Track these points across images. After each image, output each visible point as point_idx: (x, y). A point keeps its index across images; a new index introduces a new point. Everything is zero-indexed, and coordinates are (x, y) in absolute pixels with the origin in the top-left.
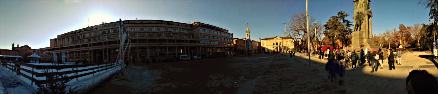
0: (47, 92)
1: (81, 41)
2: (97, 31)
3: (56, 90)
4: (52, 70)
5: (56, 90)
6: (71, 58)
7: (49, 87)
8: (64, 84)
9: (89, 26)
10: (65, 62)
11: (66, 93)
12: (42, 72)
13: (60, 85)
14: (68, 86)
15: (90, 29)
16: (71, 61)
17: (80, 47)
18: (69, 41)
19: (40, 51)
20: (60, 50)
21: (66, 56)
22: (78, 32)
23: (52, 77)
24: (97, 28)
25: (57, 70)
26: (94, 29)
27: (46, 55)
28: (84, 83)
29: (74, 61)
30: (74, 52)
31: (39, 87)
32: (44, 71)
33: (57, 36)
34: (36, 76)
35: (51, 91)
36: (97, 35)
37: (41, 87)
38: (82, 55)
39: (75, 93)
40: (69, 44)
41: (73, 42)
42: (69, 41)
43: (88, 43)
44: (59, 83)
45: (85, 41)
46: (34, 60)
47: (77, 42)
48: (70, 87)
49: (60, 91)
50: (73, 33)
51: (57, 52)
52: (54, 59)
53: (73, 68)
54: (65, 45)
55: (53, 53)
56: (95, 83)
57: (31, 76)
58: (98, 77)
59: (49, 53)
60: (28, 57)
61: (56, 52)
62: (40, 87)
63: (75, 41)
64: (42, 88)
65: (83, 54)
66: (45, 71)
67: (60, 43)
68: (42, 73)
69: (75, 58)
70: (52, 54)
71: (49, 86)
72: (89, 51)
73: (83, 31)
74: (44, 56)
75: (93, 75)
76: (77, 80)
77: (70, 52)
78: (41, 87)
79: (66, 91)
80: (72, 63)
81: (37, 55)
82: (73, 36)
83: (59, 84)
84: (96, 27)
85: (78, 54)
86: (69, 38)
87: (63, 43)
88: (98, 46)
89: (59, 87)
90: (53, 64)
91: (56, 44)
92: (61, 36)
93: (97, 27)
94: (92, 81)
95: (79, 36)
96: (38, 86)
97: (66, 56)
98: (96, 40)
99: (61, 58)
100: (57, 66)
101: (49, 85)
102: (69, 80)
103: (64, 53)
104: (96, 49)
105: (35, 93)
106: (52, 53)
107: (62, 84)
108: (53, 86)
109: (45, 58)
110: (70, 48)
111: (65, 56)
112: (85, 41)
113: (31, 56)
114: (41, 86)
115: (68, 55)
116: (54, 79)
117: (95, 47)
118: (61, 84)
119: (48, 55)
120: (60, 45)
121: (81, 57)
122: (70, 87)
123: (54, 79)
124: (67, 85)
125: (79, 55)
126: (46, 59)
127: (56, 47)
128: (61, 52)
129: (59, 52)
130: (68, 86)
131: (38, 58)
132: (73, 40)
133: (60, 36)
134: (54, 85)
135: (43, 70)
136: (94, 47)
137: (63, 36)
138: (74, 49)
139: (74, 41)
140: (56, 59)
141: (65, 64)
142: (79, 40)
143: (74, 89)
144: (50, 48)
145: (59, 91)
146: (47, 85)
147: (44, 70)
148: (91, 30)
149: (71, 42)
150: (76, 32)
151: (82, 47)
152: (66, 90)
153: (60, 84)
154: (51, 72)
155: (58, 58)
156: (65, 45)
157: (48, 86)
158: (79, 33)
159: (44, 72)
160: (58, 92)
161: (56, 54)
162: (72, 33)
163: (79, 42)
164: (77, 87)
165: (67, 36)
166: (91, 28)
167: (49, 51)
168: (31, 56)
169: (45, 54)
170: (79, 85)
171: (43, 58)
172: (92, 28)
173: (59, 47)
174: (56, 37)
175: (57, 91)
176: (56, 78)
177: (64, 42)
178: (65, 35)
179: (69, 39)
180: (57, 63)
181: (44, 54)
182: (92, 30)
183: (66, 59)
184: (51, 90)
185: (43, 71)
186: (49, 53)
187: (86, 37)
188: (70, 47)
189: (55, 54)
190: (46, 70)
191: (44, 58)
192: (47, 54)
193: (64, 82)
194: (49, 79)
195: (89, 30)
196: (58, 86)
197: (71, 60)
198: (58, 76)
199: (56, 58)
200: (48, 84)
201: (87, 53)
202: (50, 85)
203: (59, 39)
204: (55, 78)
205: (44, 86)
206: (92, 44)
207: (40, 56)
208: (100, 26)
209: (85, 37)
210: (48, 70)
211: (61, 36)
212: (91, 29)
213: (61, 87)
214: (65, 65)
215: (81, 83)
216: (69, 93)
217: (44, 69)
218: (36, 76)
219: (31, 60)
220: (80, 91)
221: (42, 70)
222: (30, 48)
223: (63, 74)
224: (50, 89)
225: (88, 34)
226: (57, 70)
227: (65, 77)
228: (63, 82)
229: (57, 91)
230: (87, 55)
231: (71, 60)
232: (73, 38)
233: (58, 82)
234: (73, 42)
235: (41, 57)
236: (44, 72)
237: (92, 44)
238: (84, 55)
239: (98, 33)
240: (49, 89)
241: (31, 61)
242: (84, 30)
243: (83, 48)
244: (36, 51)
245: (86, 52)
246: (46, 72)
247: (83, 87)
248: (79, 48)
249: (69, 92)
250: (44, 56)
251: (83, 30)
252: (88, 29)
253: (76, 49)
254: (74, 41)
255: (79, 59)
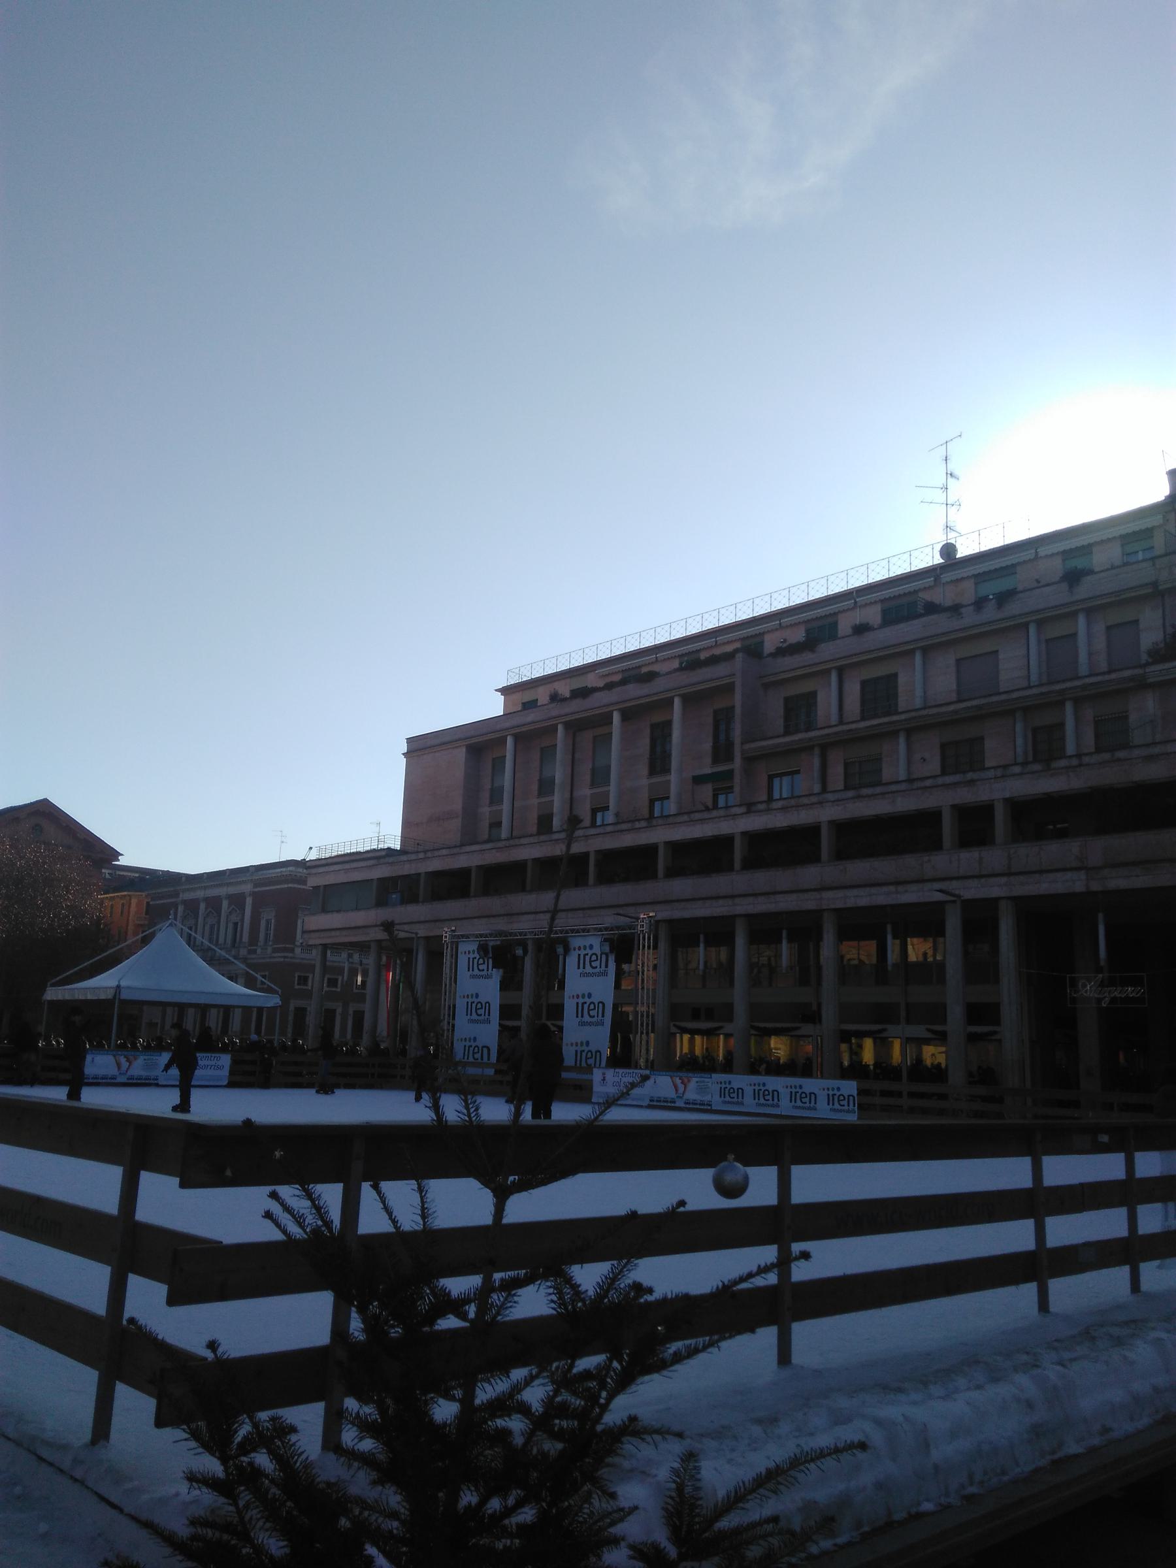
0: (344, 1522)
1: (837, 773)
2: (1090, 612)
3: (469, 1498)
4: (416, 1198)
5: (469, 1498)
6: (696, 1014)
7: (368, 1445)
8: (594, 1406)
9: (962, 552)
10: (606, 1081)
11: (615, 1541)
12: (268, 1215)
13: (541, 1423)
14: (663, 1432)
15: (968, 592)
16: (691, 1065)
17: (815, 858)
18: (659, 763)
19: (260, 901)
20: (546, 899)
21: (617, 985)
22: (798, 635)
23: (423, 1306)
24: (1079, 563)
25: (502, 1195)
26: (1039, 584)
27: (339, 959)
28: (892, 1411)
29: (728, 1066)
30: (730, 920)
31: (208, 1448)
32: (301, 1205)
33: (506, 691)
34: (173, 1300)
35: (394, 1515)
36: (1083, 669)
37: (248, 1446)
38: (847, 973)
39: (754, 1552)
40: (671, 807)
41: (729, 774)
42: (659, 763)
43: (942, 799)
44: (517, 1389)
45: (887, 774)
46: (158, 1046)
47: (782, 788)
48: (690, 1457)
49: (527, 1515)
50: (730, 656)
51: (501, 925)
52: (461, 1020)
53: (736, 1170)
54: (610, 817)
55: (446, 933)
56: (1073, 1448)
57: (96, 1302)
58: (1119, 1342)
59: (381, 935)
60: (53, 994)
61: (481, 927)
62: (224, 1460)
63: (750, 760)
64: (262, 1459)
65: (863, 952)
66: (318, 1209)
67: (546, 786)
68: (271, 1234)
69: (740, 1010)
70: (435, 952)
71: (366, 1427)
72: (953, 924)
73: (861, 629)
74: (316, 980)
75: (1043, 1304)
76: (784, 1356)
77: (670, 922)
78: (248, 1446)
79: (625, 1513)
80: (695, 1087)
81: (211, 960)
82: (729, 688)
83: (524, 1409)
84: (1066, 554)
85: (786, 952)
86: (669, 723)
87: (585, 791)
88: (1097, 848)
89: (519, 1441)
90: (436, 1107)
91: (485, 810)
92: (554, 698)
93: (1086, 550)
94: (1030, 1405)
95: (810, 699)
96: (195, 1435)
97: (619, 974)
98: (1070, 749)
99: (557, 1011)
100: (496, 1132)
101: (369, 1411)
102: (674, 1347)
103: (595, 943)
104: (1076, 883)
105: (149, 1551)
106: (422, 931)
107: (563, 1410)
108: (437, 1430)
109: (330, 1015)
110: (671, 873)
111: (603, 989)
112: (895, 767)
113: (103, 983)
114: (244, 1430)
115: (649, 974)
116: (450, 1322)
117: (1053, 851)
118: (549, 1403)
119: (370, 961)
120: (545, 823)
121: (829, 1012)
122: (690, 1457)
123: (450, 1322)
124: (632, 1428)
125: (807, 972)
126: (341, 1032)
127: (493, 857)
128: (562, 921)
129: (524, 926)
130: (663, 1432)
131: (227, 1010)
132: (722, 752)
133: (542, 695)
134: (445, 1411)
135: (287, 1192)
136: (1028, 853)
137: (583, 693)
138: (737, 881)
139: (737, 764)
140: (488, 1034)
141: (610, 1103)
142: (807, 748)
143: (737, 1499)
144: (407, 870)
145: (520, 1504)
146: (334, 1419)
147: (309, 1196)
148: (980, 603)
149: (698, 780)
150: (770, 645)
151: (752, 863)
152: (624, 1503)
153: (535, 1395)
154: (410, 1221)
155: (508, 1011)
156: (610, 817)
157: (349, 1436)
158: (807, 657)
159: (294, 1230)
160: (498, 1518)
161: (483, 949)
162: (714, 660)
163: (807, 782)
164: (797, 1462)
165: (634, 691)
166: (980, 578)
167: (381, 902)
168: (103, 983)
169: (337, 947)
170: (824, 1440)
171: (301, 1013)
172: (1010, 570)
173: (529, 852)
174: (494, 707)
175: (495, 1504)
176: (472, 1310)
177: (600, 776)
178: (609, 686)
179: (661, 733)
180: (492, 1089)
181: (315, 954)
182: (1003, 598)
183: (622, 1028)
184: (393, 1498)
185: (287, 1209)
186: (381, 935)
187: (902, 704)
188: (677, 848)
189: (468, 949)
190: (331, 1194)
191: (311, 1021)
192: (362, 947)
193: (598, 1375)
194: (373, 1326)
195: (955, 609)
196: (506, 1433)
197: (682, 1045)
198: (511, 1286)
199: (478, 1009)
200: (360, 1399)
201: (916, 949)
202: (382, 1410)
203: (524, 738)
204: (455, 1306)
205: (293, 1429)
206: (1000, 816)
207: (250, 983)
208: (1126, 539)
209: (892, 710)
210: (366, 1187)
211: (554, 698)
212: (991, 588)
213: (553, 1447)
214: (617, 1115)
215: (840, 1419)
216: (672, 1552)
217: (304, 1178)
218: (173, 1300)
219: (99, 1047)
220: (826, 1544)
221: (274, 1195)
222: (102, 854)
223: (587, 1256)
224: (386, 1473)
225: (945, 663)
226: (502, 1195)
227: (613, 1296)
228: (587, 1375)
229: (495, 1504)
230: (930, 972)
231: (682, 1045)
232: (723, 719)
233: (502, 1367)
234: (721, 782)
235: (274, 1001)
236: (299, 1220)
237: (1000, 816)
238: (881, 973)
239: (1100, 643)
240: (360, 1483)
241: (98, 1063)
242: (873, 615)
243: (858, 869)
244: (192, 907)
245: (902, 935)
246: (328, 1224)
247: (879, 1486)
248: (810, 874)
249: (660, 1536)
250: (316, 980)
251: (858, 617)
252: (940, 596)
253: (761, 879)
254: (737, 764)
255: (807, 1029)
